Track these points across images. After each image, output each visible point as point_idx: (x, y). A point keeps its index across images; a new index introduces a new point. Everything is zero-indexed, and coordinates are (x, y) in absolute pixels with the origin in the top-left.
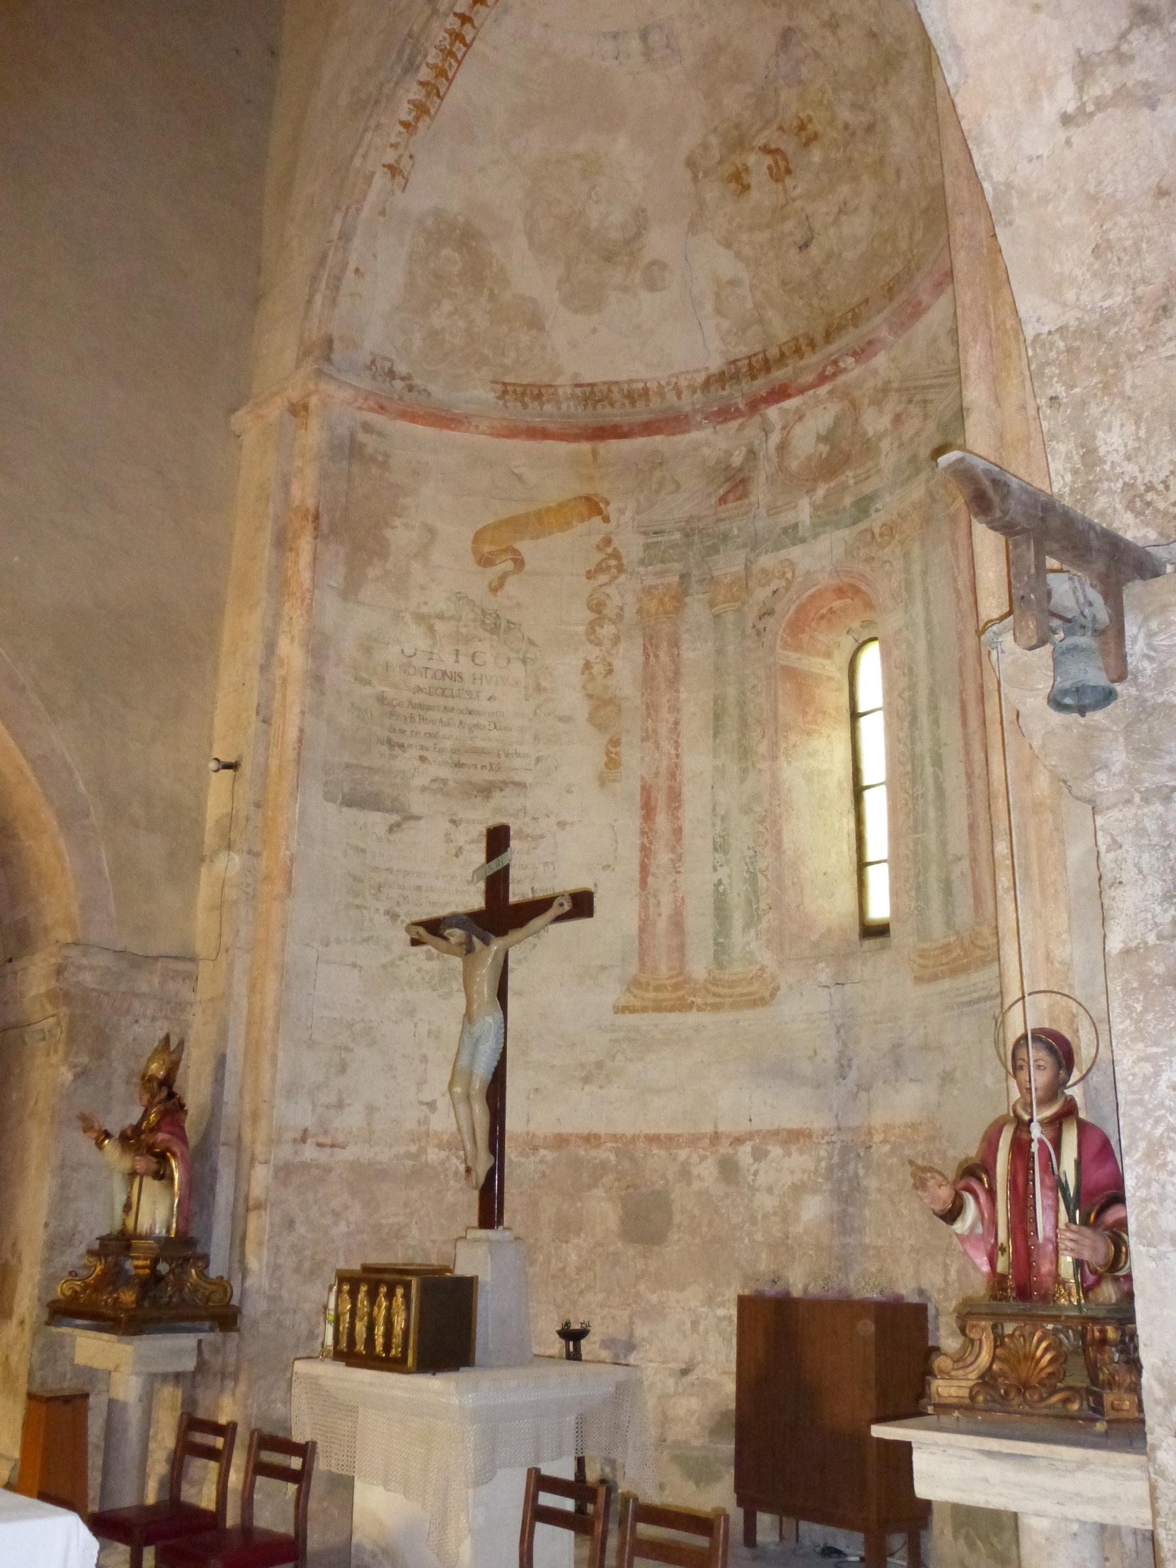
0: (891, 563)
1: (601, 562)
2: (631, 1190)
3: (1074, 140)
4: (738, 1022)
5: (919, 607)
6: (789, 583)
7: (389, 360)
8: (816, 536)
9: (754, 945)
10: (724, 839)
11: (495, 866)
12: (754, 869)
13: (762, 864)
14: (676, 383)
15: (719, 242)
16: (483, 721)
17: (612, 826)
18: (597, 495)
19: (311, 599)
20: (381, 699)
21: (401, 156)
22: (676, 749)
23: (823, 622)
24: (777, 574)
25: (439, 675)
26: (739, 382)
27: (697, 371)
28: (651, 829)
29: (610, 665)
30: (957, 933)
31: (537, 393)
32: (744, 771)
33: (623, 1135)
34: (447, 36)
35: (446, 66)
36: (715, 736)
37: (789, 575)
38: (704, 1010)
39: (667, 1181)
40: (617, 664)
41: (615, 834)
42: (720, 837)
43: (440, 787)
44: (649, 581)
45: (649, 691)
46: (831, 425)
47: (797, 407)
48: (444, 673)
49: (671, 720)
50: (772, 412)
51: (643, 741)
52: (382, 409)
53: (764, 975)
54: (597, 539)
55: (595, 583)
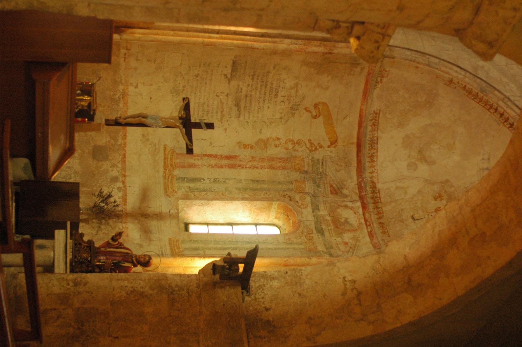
0: (300, 239)
1: (314, 144)
2: (109, 149)
3: (340, 280)
4: (160, 184)
5: (284, 246)
6: (300, 207)
7: (387, 76)
8: (314, 216)
9: (183, 190)
10: (218, 182)
11: (203, 125)
12: (208, 191)
13: (209, 193)
14: (375, 172)
15: (420, 189)
16: (261, 104)
17: (224, 146)
18: (338, 144)
19: (302, 52)
20: (269, 72)
21: (455, 84)
22: (248, 167)
23: (286, 217)
24: (303, 202)
25: (277, 90)
26: (372, 193)
27: (378, 179)
28: (223, 158)
29: (278, 146)
30: (183, 251)
31: (375, 124)
32: (239, 189)
33: (126, 147)
34: (491, 103)
35: (482, 102)
36: (251, 180)
37: (302, 207)
38: (164, 173)
39: (112, 160)
40: (278, 149)
41: (222, 146)
42: (219, 181)
43: (239, 90)
44: (306, 160)
45: (269, 159)
46: (350, 223)
47: (359, 212)
48: (277, 92)
49: (258, 166)
50: (359, 204)
51: (252, 157)
52: (369, 74)
53: (174, 193)
54: (322, 143)
55: (307, 142)
